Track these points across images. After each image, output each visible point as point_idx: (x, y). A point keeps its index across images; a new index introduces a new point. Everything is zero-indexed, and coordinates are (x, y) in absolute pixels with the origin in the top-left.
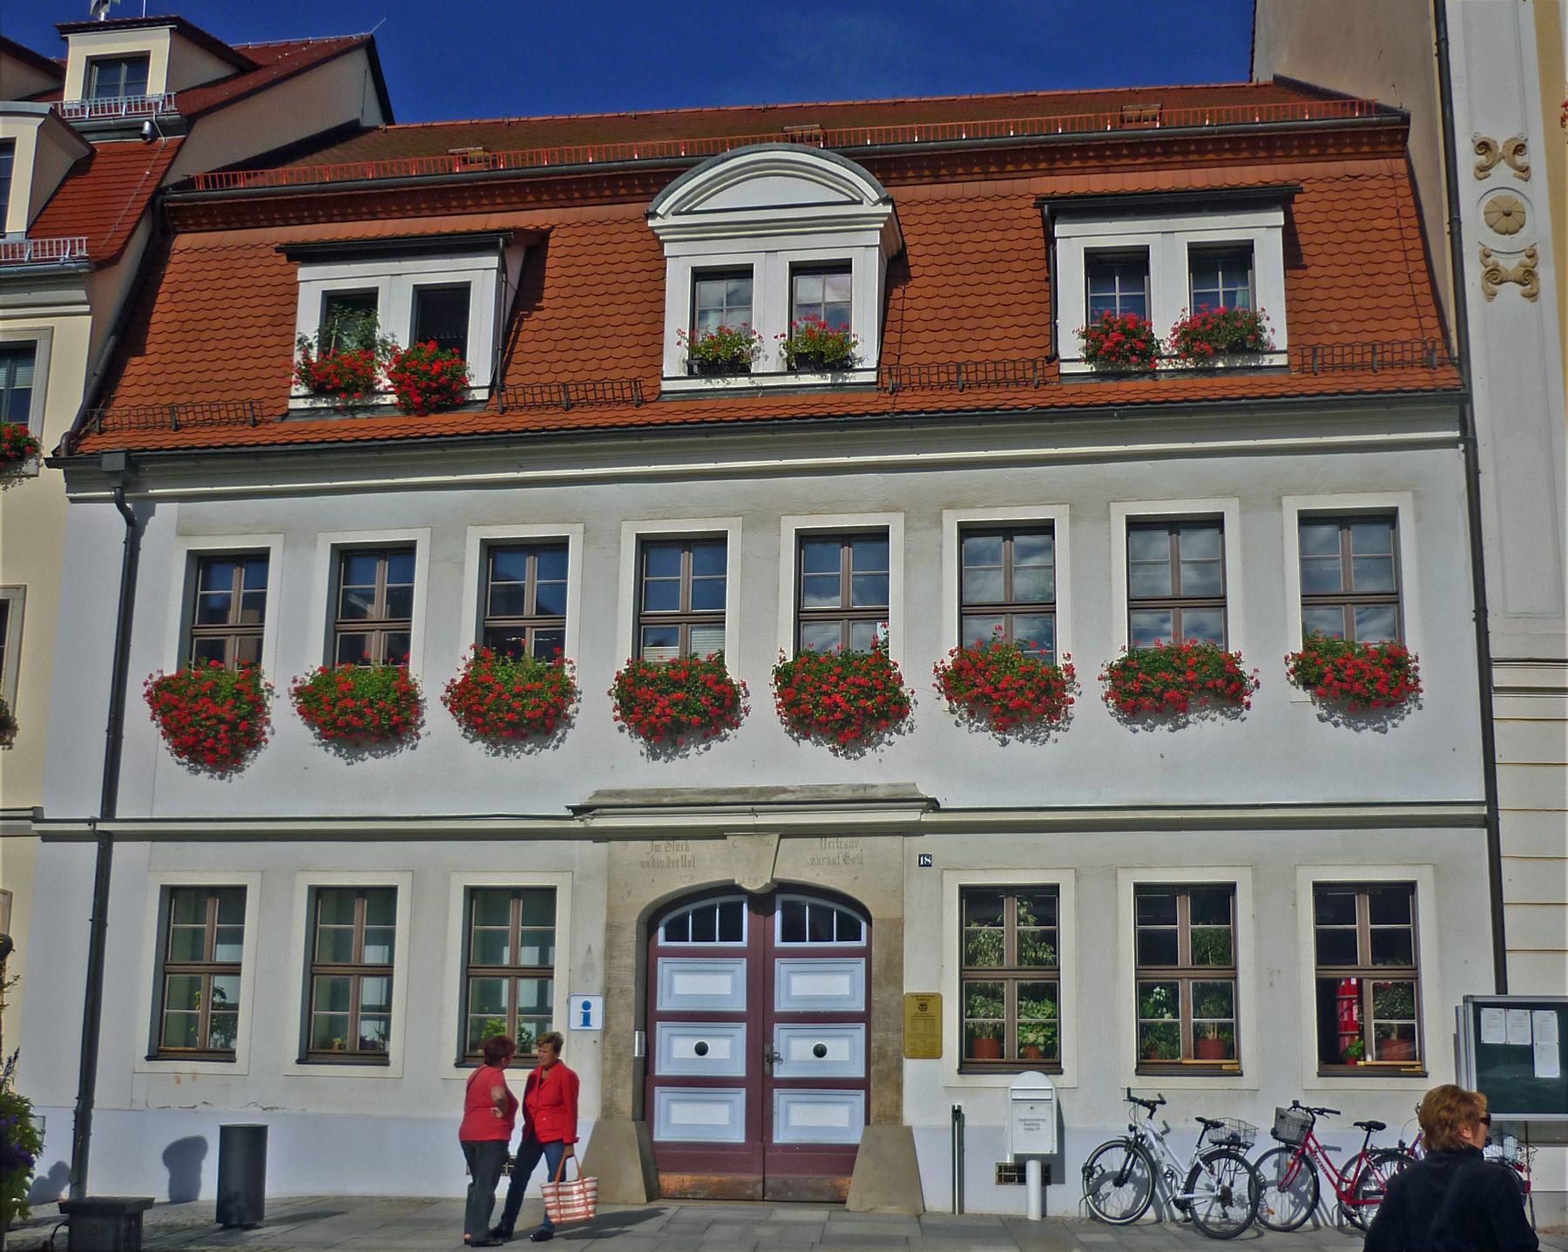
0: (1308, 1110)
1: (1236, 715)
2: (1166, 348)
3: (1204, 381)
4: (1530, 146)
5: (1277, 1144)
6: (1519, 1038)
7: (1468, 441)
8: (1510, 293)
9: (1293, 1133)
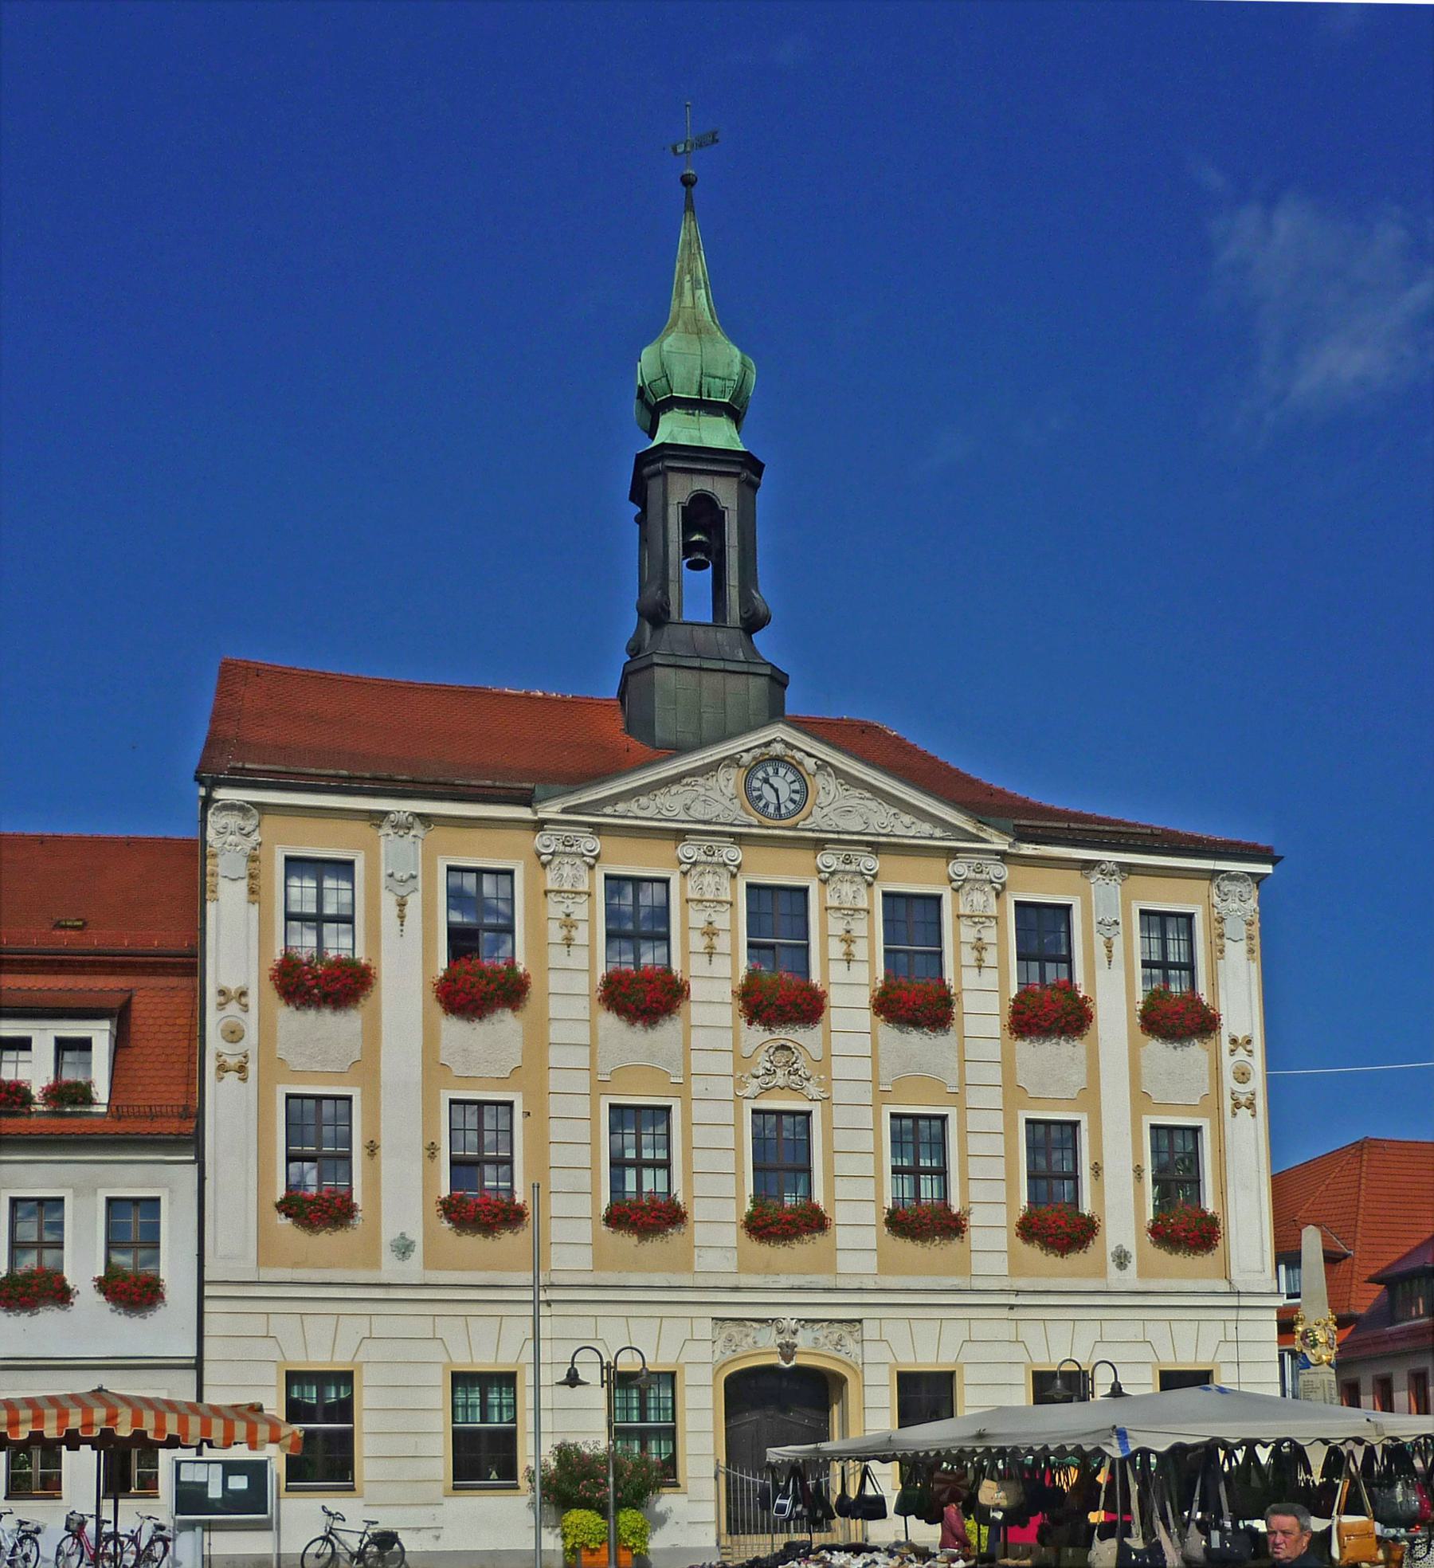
0: (82, 1515)
1: (65, 1309)
2: (37, 1099)
3: (55, 1121)
4: (250, 992)
5: (67, 1533)
6: (200, 1478)
7: (200, 1161)
8: (232, 1077)
9: (74, 1526)
